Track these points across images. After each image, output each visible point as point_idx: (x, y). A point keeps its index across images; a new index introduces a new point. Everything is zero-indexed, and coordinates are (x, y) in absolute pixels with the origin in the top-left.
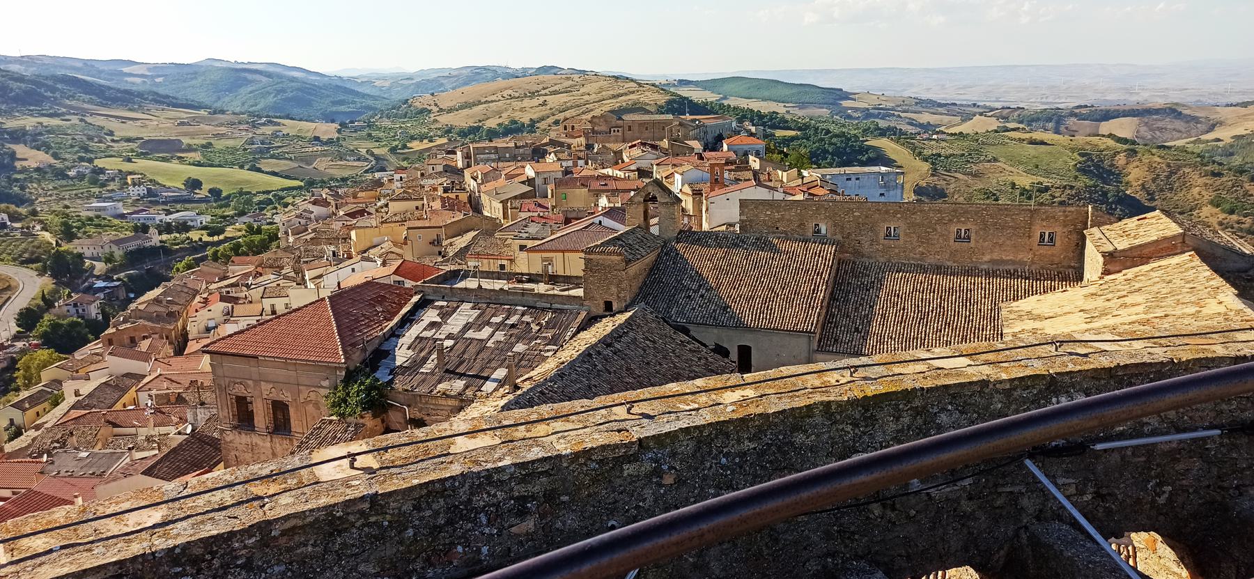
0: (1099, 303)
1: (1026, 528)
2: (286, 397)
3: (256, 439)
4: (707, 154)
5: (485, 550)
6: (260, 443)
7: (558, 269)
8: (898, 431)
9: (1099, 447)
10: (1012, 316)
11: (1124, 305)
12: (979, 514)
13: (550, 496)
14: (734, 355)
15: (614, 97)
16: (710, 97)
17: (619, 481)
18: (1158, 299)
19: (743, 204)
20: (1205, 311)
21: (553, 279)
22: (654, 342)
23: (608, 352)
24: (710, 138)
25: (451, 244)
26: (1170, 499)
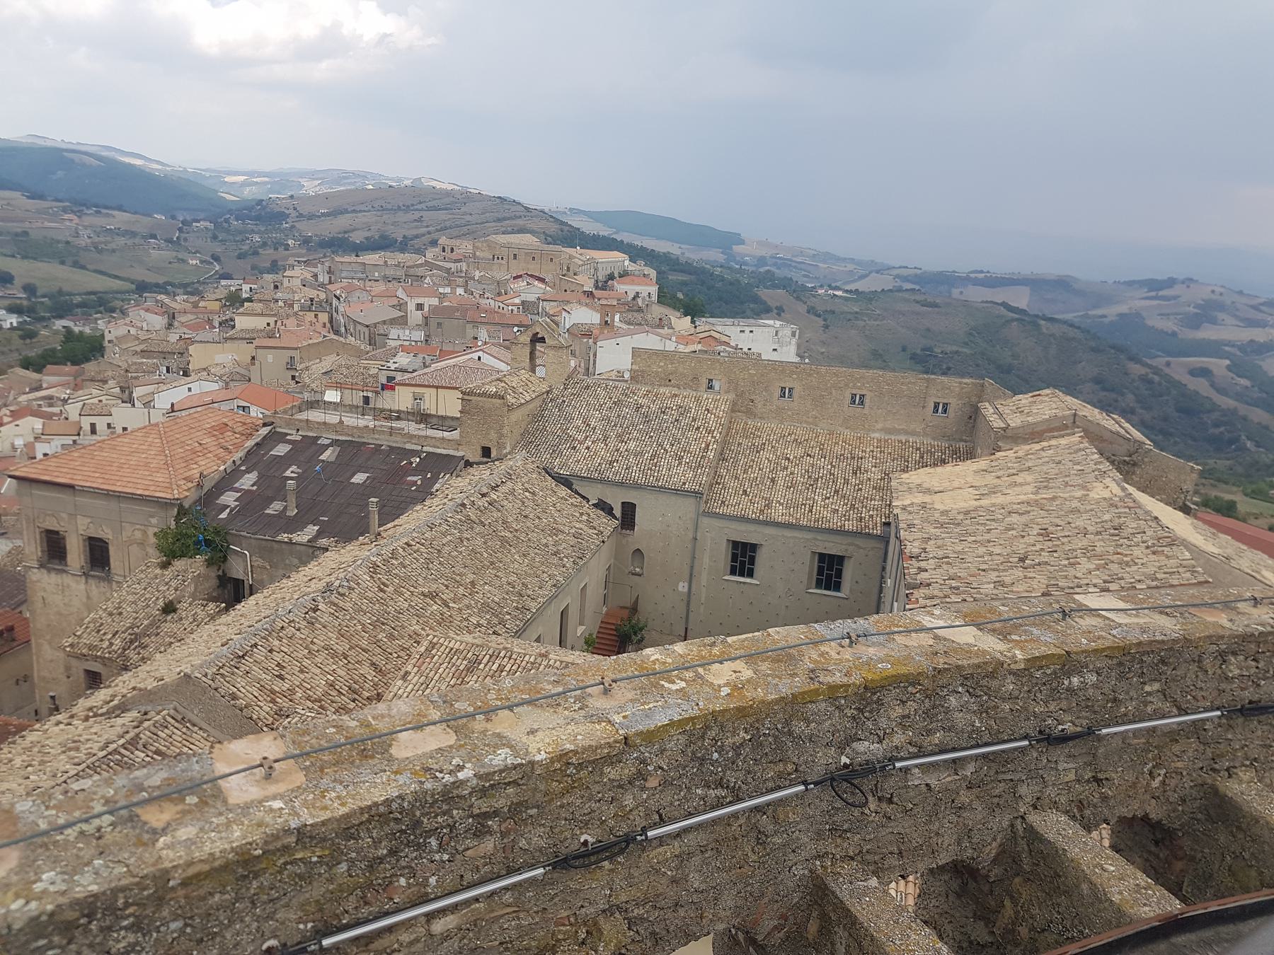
0: (990, 479)
1: (1022, 817)
2: (105, 533)
3: (67, 579)
4: (597, 293)
5: (433, 880)
6: (73, 585)
7: (429, 405)
8: (904, 717)
9: (1104, 731)
10: (901, 488)
11: (1015, 484)
12: (976, 804)
13: (516, 809)
14: (618, 512)
15: (499, 220)
16: (604, 231)
17: (597, 788)
18: (1045, 483)
19: (636, 352)
20: (1093, 495)
21: (424, 418)
22: (533, 494)
23: (482, 502)
24: (601, 276)
25: (307, 368)
26: (1163, 783)
